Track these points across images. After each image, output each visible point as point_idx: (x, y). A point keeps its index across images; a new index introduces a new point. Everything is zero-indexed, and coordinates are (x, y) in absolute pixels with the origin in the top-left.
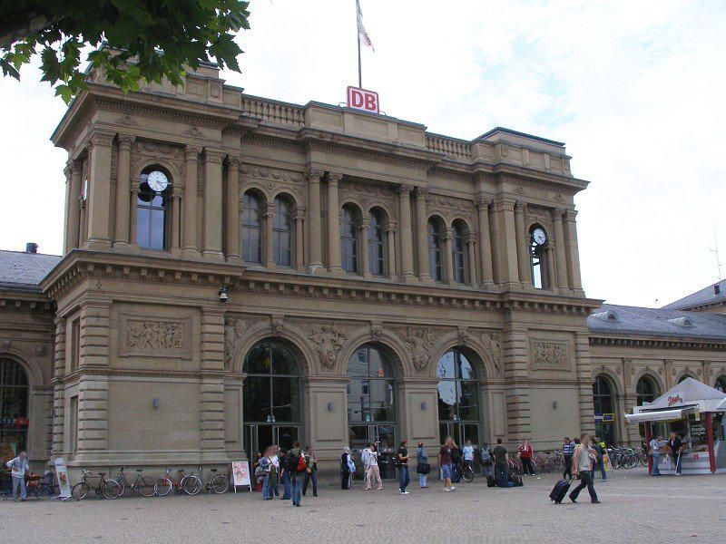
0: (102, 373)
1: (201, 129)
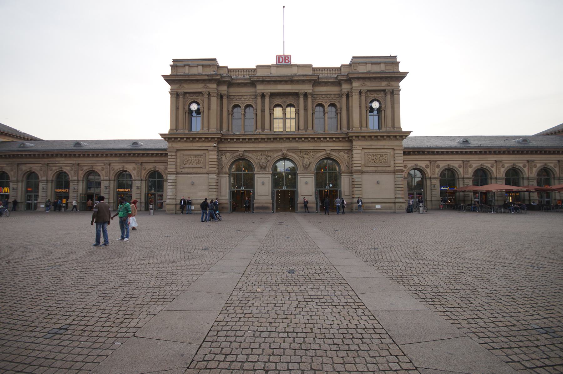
0: (173, 174)
1: (208, 85)
